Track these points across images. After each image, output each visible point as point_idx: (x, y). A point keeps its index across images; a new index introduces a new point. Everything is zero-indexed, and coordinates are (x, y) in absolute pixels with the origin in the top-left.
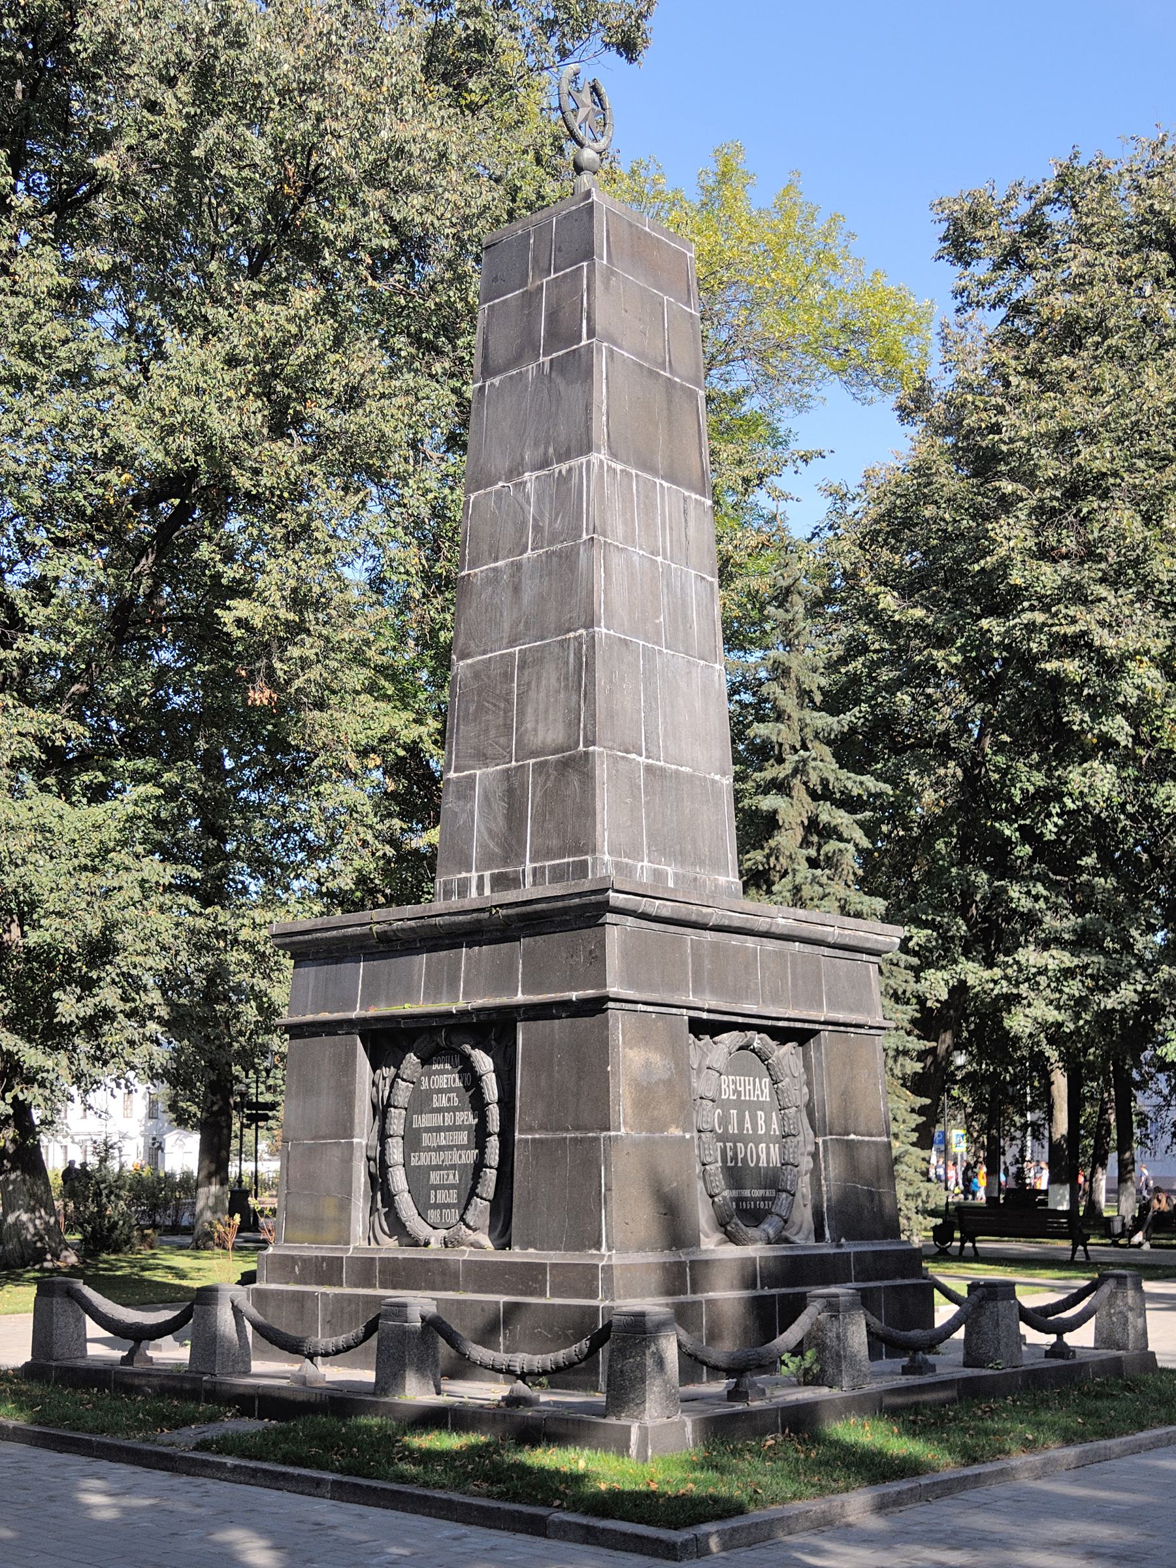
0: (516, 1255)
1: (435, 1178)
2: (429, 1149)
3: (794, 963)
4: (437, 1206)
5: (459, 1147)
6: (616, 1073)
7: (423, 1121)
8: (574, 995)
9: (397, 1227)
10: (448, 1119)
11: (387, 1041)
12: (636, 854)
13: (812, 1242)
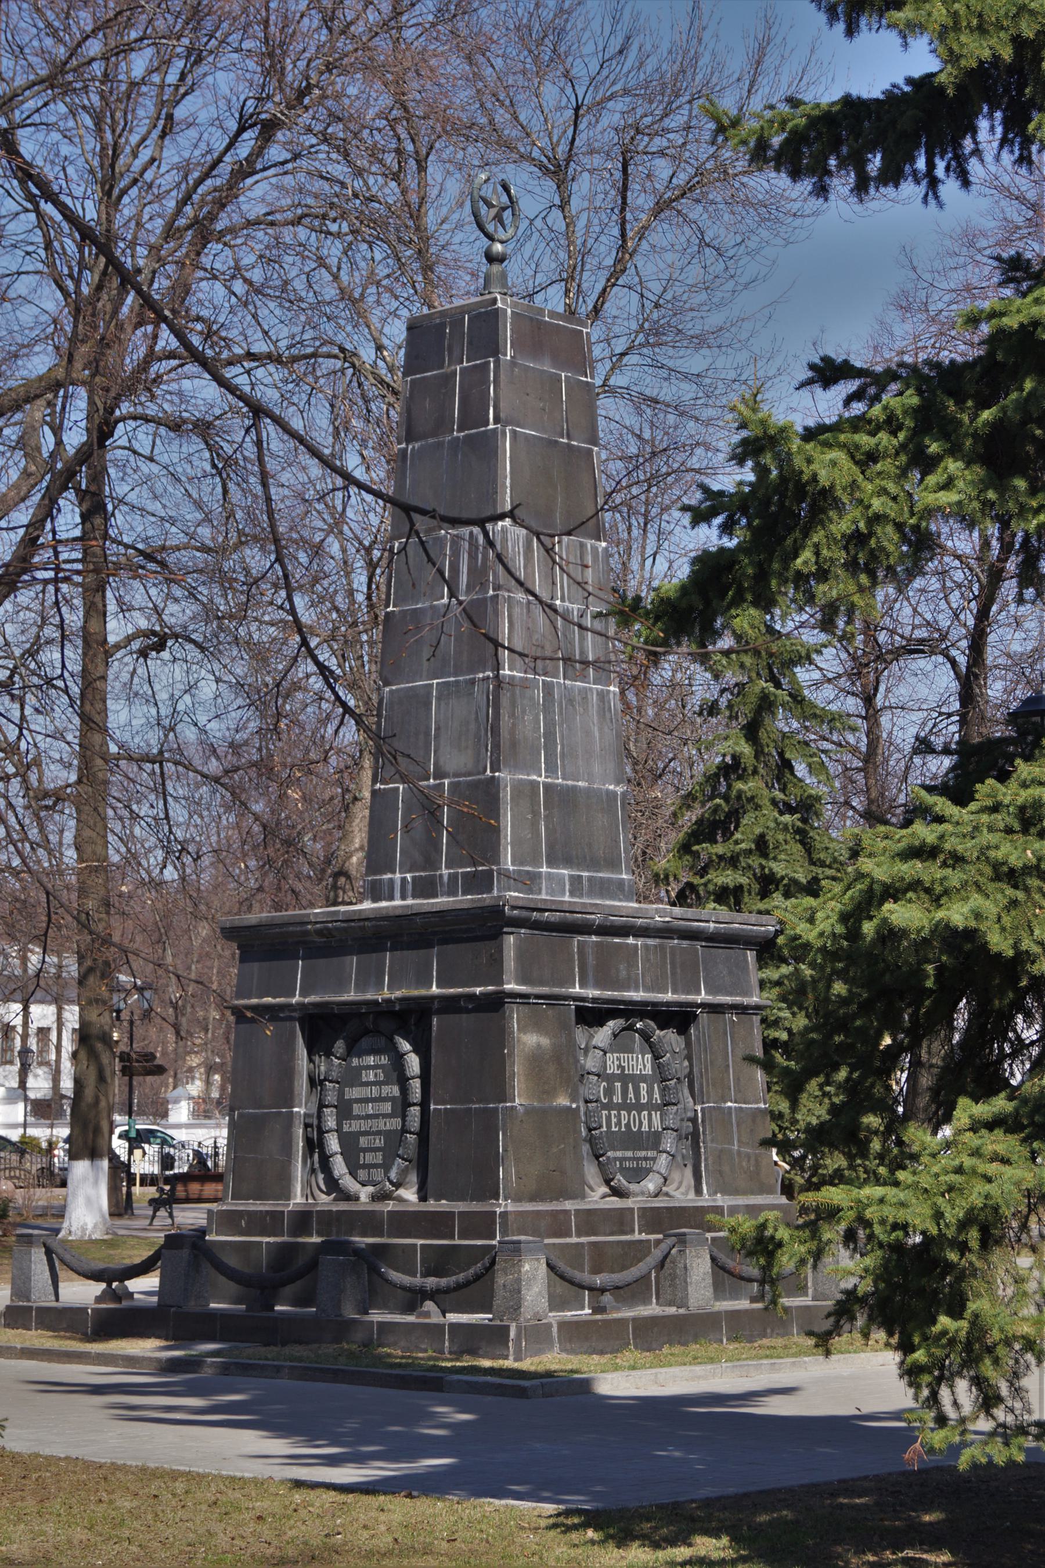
0: (432, 1205)
1: (363, 1142)
2: (359, 1117)
3: (673, 954)
4: (365, 1166)
5: (385, 1116)
6: (511, 1054)
7: (354, 1093)
8: (478, 990)
9: (333, 1185)
10: (374, 1091)
11: (323, 1027)
12: (536, 862)
13: (692, 1195)
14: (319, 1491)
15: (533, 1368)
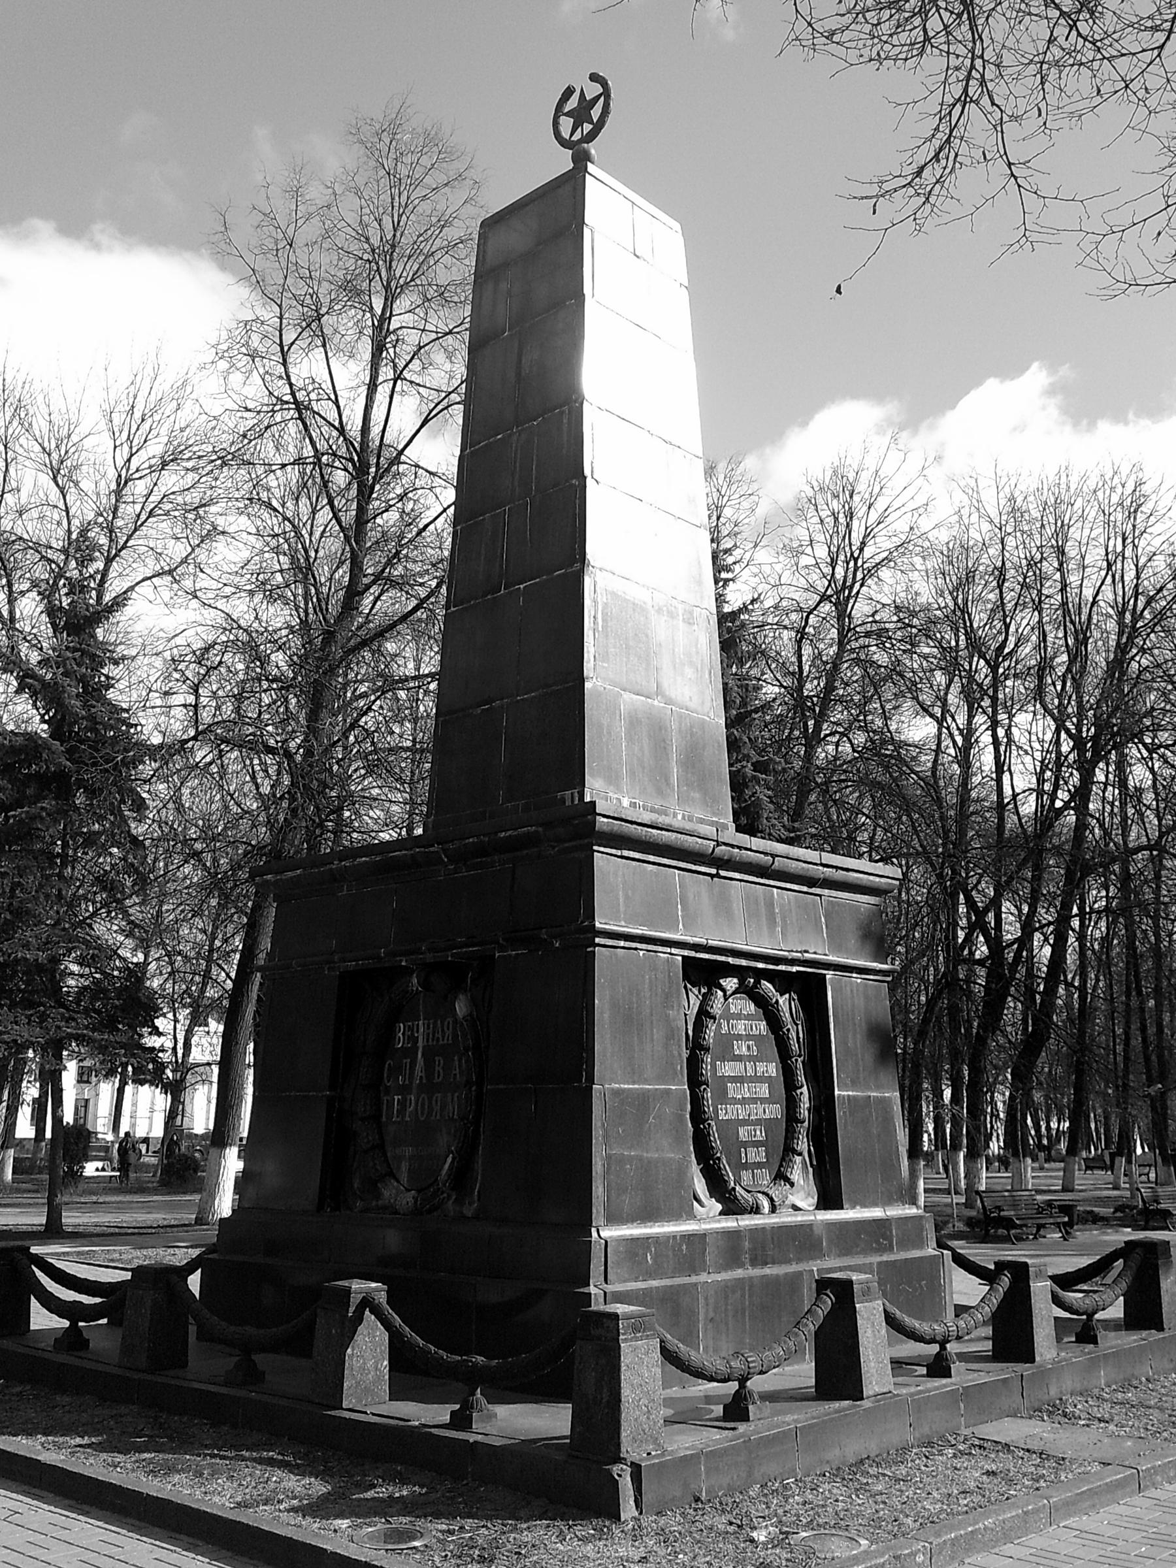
2: (735, 1101)
5: (763, 1100)
14: (388, 399)
15: (277, 1474)
